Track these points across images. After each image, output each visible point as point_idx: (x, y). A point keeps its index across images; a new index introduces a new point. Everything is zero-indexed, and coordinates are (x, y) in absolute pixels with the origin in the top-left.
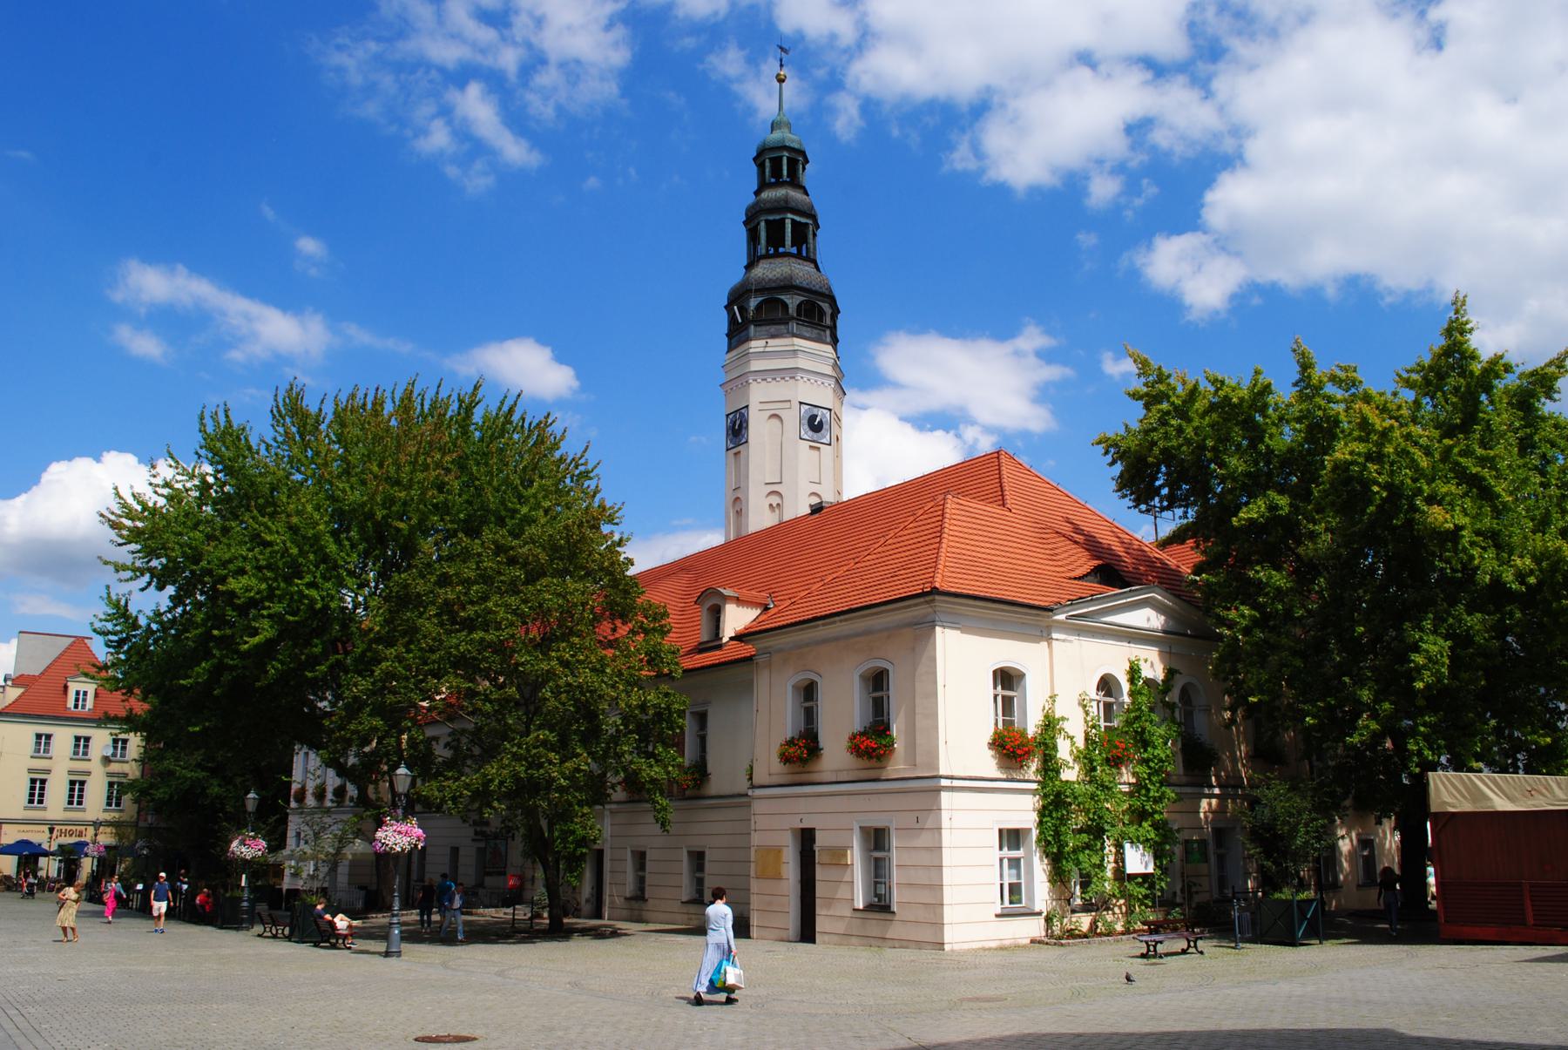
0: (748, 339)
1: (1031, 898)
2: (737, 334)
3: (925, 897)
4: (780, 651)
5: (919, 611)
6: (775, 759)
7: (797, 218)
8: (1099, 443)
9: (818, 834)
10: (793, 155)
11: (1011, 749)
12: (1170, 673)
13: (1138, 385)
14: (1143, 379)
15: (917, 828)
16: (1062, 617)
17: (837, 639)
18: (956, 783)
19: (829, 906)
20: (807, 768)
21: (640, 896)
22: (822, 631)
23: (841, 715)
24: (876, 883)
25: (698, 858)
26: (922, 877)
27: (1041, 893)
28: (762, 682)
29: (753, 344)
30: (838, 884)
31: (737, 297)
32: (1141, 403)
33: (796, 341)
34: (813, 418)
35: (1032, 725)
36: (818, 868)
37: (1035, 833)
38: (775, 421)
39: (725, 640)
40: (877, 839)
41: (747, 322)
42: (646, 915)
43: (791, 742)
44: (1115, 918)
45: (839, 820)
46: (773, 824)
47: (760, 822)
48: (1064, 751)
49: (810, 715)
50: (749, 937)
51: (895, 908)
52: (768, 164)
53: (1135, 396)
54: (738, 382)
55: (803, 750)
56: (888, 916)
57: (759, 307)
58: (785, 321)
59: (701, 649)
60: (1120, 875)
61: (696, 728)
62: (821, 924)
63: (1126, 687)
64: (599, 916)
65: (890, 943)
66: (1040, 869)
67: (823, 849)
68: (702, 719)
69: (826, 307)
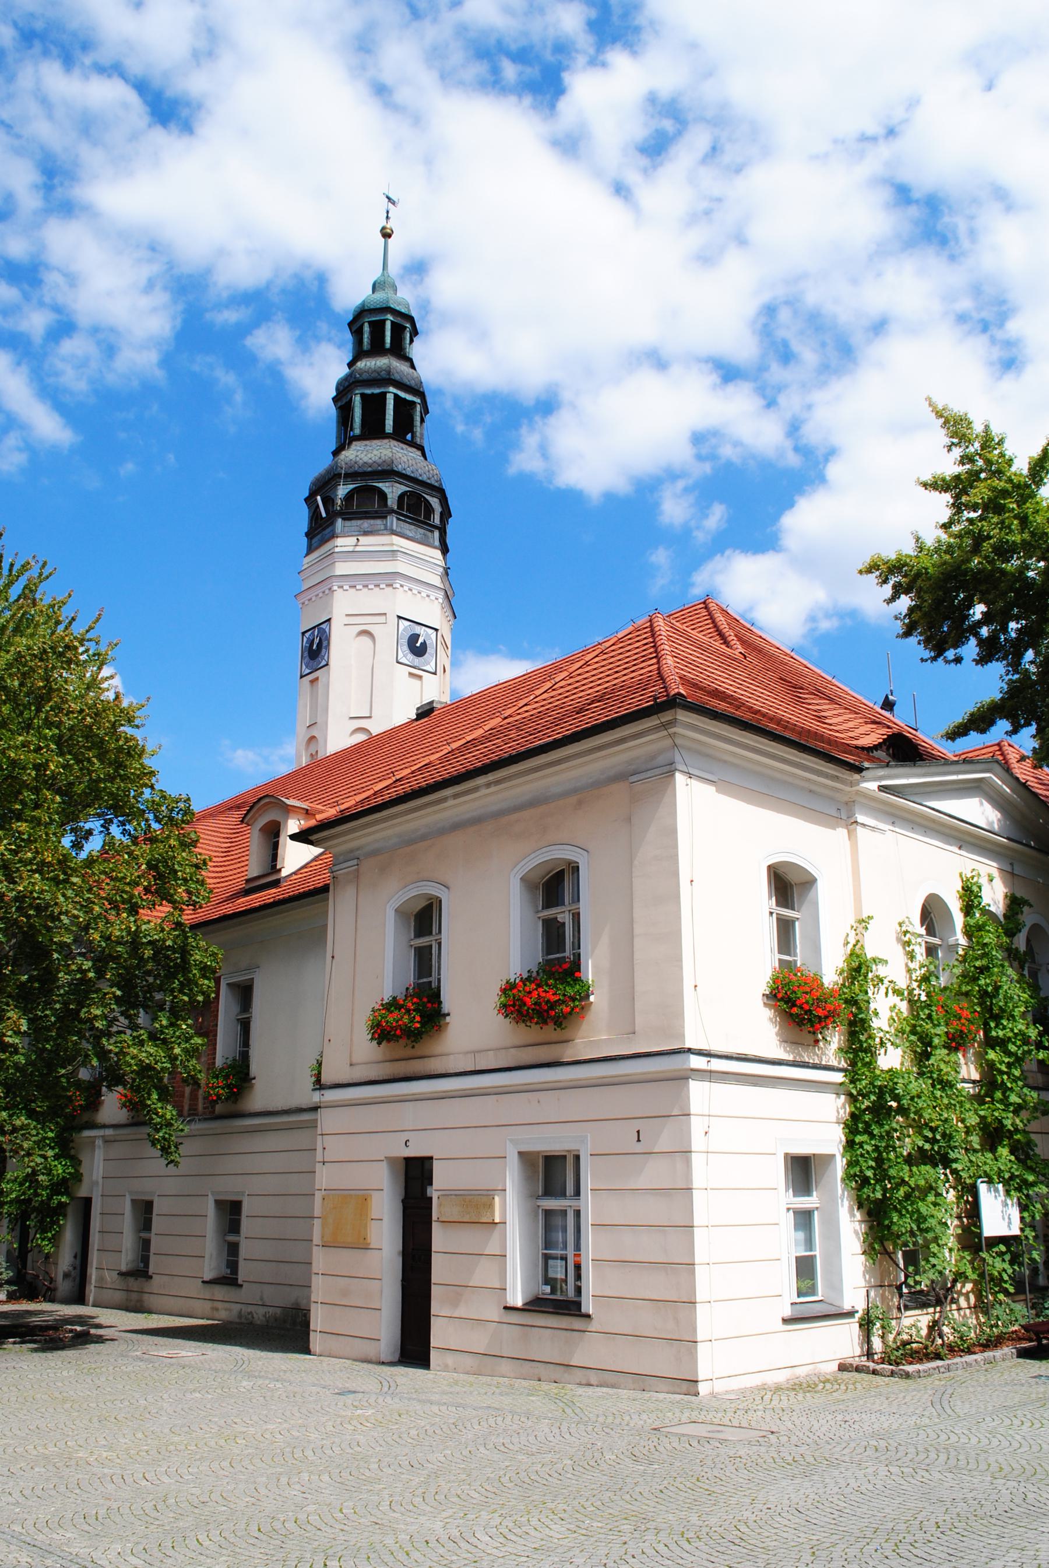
0: (333, 536)
1: (836, 1286)
2: (319, 531)
3: (657, 1286)
4: (375, 853)
5: (641, 744)
6: (362, 1034)
7: (402, 394)
8: (869, 570)
9: (437, 1166)
10: (399, 320)
11: (799, 1008)
12: (1014, 903)
13: (949, 466)
14: (957, 452)
15: (641, 1149)
16: (872, 786)
17: (476, 821)
18: (717, 1065)
19: (455, 1303)
20: (420, 1049)
21: (140, 1272)
22: (454, 806)
23: (487, 948)
24: (547, 1258)
25: (231, 1212)
26: (648, 1247)
27: (852, 1278)
28: (342, 913)
29: (339, 541)
30: (499, 1270)
31: (323, 486)
32: (947, 498)
33: (396, 539)
34: (413, 639)
35: (830, 972)
36: (437, 1230)
37: (840, 1164)
38: (365, 639)
39: (284, 873)
40: (552, 1175)
41: (332, 516)
42: (151, 1301)
43: (393, 1005)
44: (962, 1316)
45: (478, 1145)
46: (355, 1155)
47: (331, 1147)
48: (885, 1010)
49: (425, 961)
50: (308, 1351)
51: (588, 1306)
52: (366, 328)
53: (938, 485)
54: (318, 590)
55: (413, 1020)
56: (577, 1323)
57: (349, 497)
58: (382, 513)
59: (252, 887)
60: (972, 1239)
61: (235, 1009)
62: (440, 1333)
63: (959, 919)
64: (80, 1299)
65: (579, 1375)
66: (850, 1228)
67: (448, 1194)
68: (245, 993)
69: (435, 502)
